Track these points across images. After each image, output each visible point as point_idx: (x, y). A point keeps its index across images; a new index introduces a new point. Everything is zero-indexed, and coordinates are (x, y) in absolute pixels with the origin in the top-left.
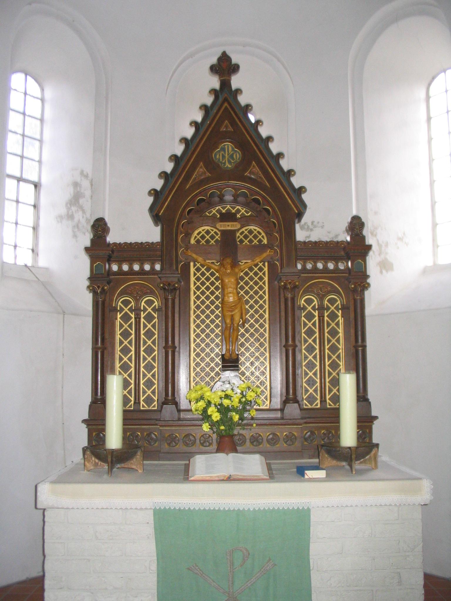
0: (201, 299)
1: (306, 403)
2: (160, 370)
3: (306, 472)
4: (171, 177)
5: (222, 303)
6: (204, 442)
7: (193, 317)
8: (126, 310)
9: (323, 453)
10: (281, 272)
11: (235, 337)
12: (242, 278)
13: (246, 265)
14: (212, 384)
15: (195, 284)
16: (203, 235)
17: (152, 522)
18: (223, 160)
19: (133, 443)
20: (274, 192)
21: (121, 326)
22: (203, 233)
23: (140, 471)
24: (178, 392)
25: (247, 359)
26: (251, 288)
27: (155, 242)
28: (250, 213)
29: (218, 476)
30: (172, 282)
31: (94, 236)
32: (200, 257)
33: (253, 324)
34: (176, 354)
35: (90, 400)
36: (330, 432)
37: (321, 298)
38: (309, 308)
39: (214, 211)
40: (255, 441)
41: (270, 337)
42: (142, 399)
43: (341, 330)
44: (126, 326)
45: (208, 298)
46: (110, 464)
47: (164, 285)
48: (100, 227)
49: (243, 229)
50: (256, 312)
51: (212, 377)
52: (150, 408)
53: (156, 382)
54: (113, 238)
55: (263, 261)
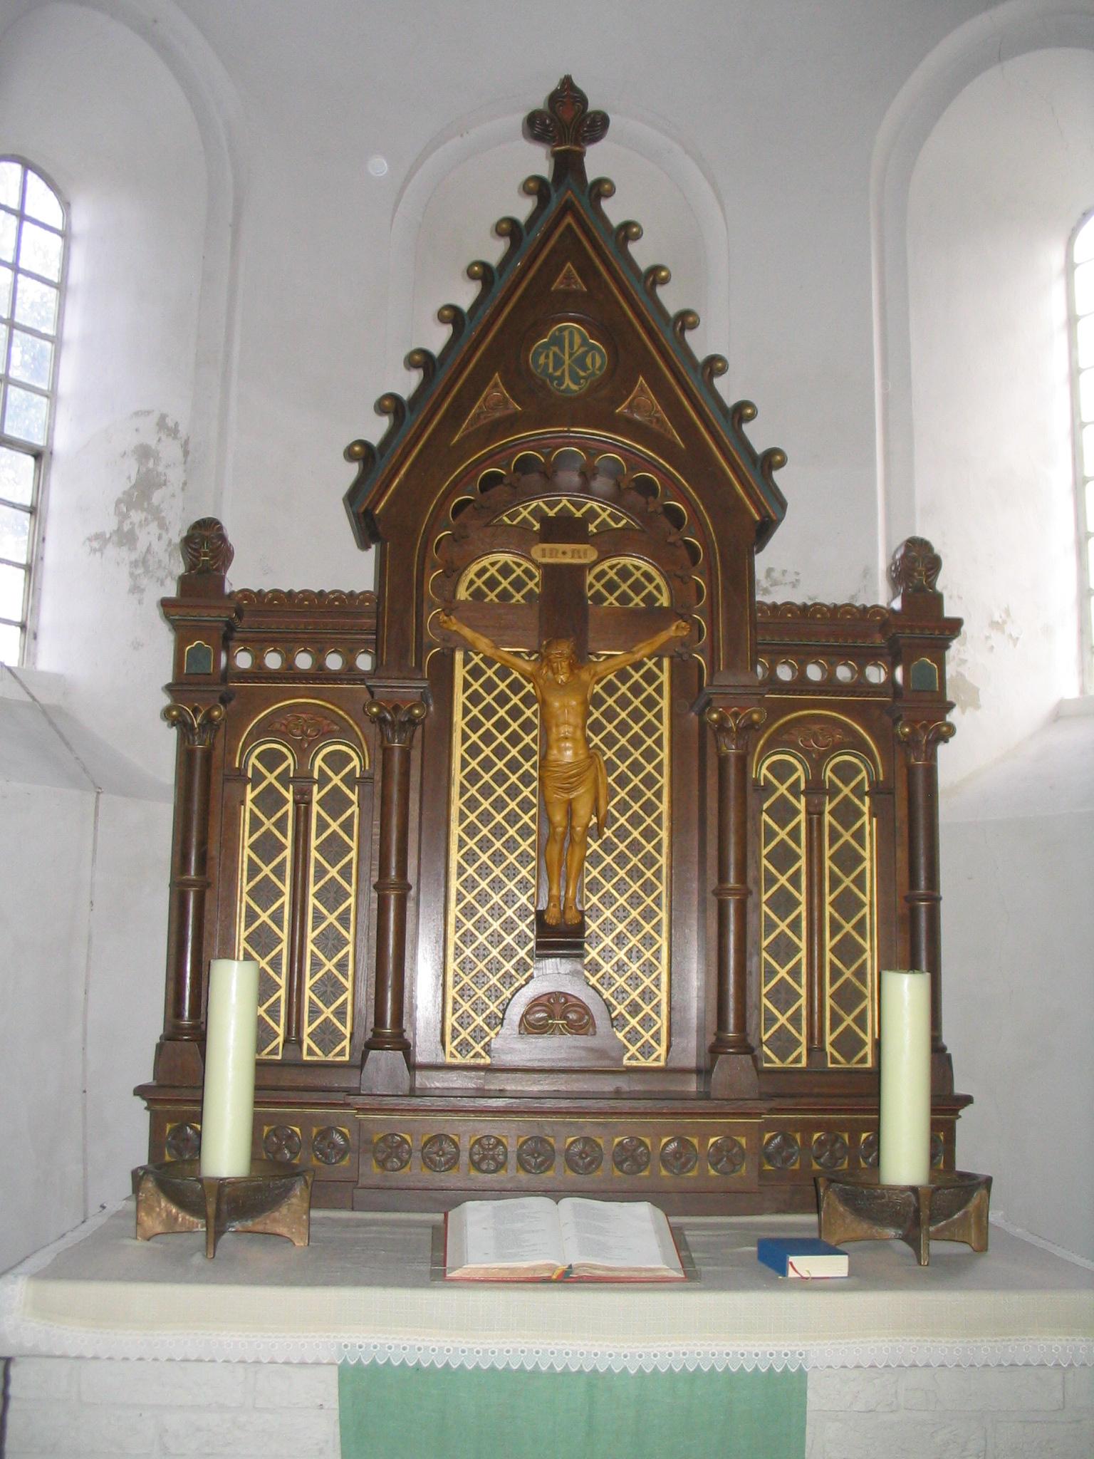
0: (482, 756)
1: (769, 1052)
2: (363, 951)
3: (792, 1259)
4: (412, 411)
5: (543, 765)
6: (484, 1158)
7: (457, 804)
8: (271, 778)
9: (830, 1198)
10: (710, 684)
11: (575, 865)
12: (597, 701)
13: (612, 662)
14: (507, 994)
15: (466, 711)
16: (492, 578)
17: (333, 1403)
18: (555, 369)
19: (278, 1156)
20: (697, 463)
21: (256, 823)
22: (493, 571)
23: (300, 1243)
24: (708, 965)
25: (607, 927)
26: (623, 728)
27: (358, 591)
28: (624, 522)
29: (534, 1269)
30: (405, 701)
31: (191, 566)
32: (486, 636)
33: (626, 830)
34: (410, 905)
35: (160, 1031)
36: (837, 1138)
37: (816, 765)
38: (783, 789)
39: (525, 513)
40: (626, 1160)
41: (671, 867)
42: (307, 1030)
43: (868, 853)
44: (268, 824)
45: (500, 752)
46: (212, 1222)
47: (381, 708)
48: (206, 546)
49: (605, 566)
50: (635, 794)
51: (508, 975)
52: (330, 1058)
53: (348, 984)
54: (240, 577)
55: (658, 655)
